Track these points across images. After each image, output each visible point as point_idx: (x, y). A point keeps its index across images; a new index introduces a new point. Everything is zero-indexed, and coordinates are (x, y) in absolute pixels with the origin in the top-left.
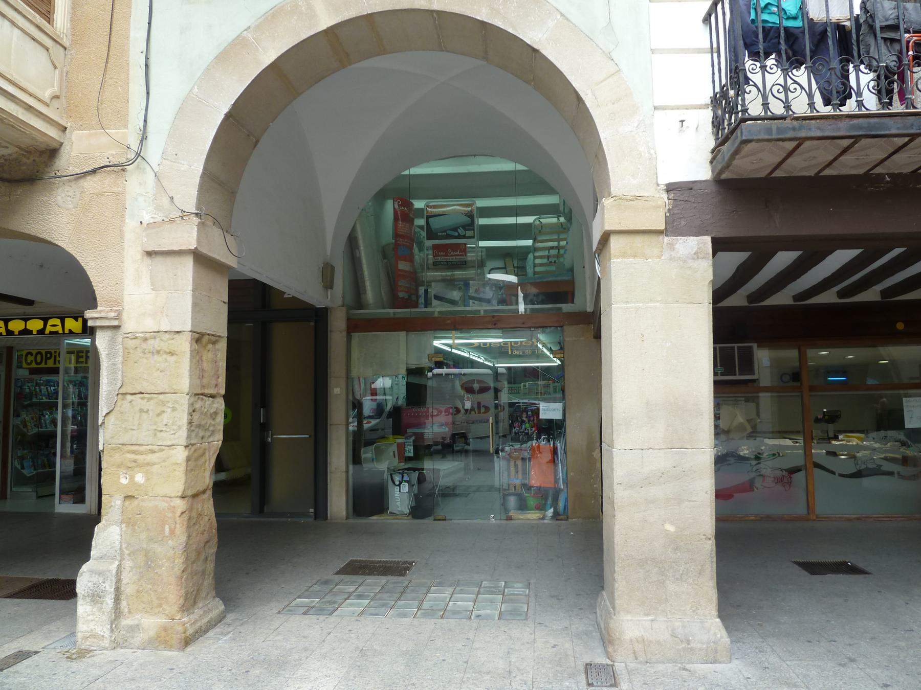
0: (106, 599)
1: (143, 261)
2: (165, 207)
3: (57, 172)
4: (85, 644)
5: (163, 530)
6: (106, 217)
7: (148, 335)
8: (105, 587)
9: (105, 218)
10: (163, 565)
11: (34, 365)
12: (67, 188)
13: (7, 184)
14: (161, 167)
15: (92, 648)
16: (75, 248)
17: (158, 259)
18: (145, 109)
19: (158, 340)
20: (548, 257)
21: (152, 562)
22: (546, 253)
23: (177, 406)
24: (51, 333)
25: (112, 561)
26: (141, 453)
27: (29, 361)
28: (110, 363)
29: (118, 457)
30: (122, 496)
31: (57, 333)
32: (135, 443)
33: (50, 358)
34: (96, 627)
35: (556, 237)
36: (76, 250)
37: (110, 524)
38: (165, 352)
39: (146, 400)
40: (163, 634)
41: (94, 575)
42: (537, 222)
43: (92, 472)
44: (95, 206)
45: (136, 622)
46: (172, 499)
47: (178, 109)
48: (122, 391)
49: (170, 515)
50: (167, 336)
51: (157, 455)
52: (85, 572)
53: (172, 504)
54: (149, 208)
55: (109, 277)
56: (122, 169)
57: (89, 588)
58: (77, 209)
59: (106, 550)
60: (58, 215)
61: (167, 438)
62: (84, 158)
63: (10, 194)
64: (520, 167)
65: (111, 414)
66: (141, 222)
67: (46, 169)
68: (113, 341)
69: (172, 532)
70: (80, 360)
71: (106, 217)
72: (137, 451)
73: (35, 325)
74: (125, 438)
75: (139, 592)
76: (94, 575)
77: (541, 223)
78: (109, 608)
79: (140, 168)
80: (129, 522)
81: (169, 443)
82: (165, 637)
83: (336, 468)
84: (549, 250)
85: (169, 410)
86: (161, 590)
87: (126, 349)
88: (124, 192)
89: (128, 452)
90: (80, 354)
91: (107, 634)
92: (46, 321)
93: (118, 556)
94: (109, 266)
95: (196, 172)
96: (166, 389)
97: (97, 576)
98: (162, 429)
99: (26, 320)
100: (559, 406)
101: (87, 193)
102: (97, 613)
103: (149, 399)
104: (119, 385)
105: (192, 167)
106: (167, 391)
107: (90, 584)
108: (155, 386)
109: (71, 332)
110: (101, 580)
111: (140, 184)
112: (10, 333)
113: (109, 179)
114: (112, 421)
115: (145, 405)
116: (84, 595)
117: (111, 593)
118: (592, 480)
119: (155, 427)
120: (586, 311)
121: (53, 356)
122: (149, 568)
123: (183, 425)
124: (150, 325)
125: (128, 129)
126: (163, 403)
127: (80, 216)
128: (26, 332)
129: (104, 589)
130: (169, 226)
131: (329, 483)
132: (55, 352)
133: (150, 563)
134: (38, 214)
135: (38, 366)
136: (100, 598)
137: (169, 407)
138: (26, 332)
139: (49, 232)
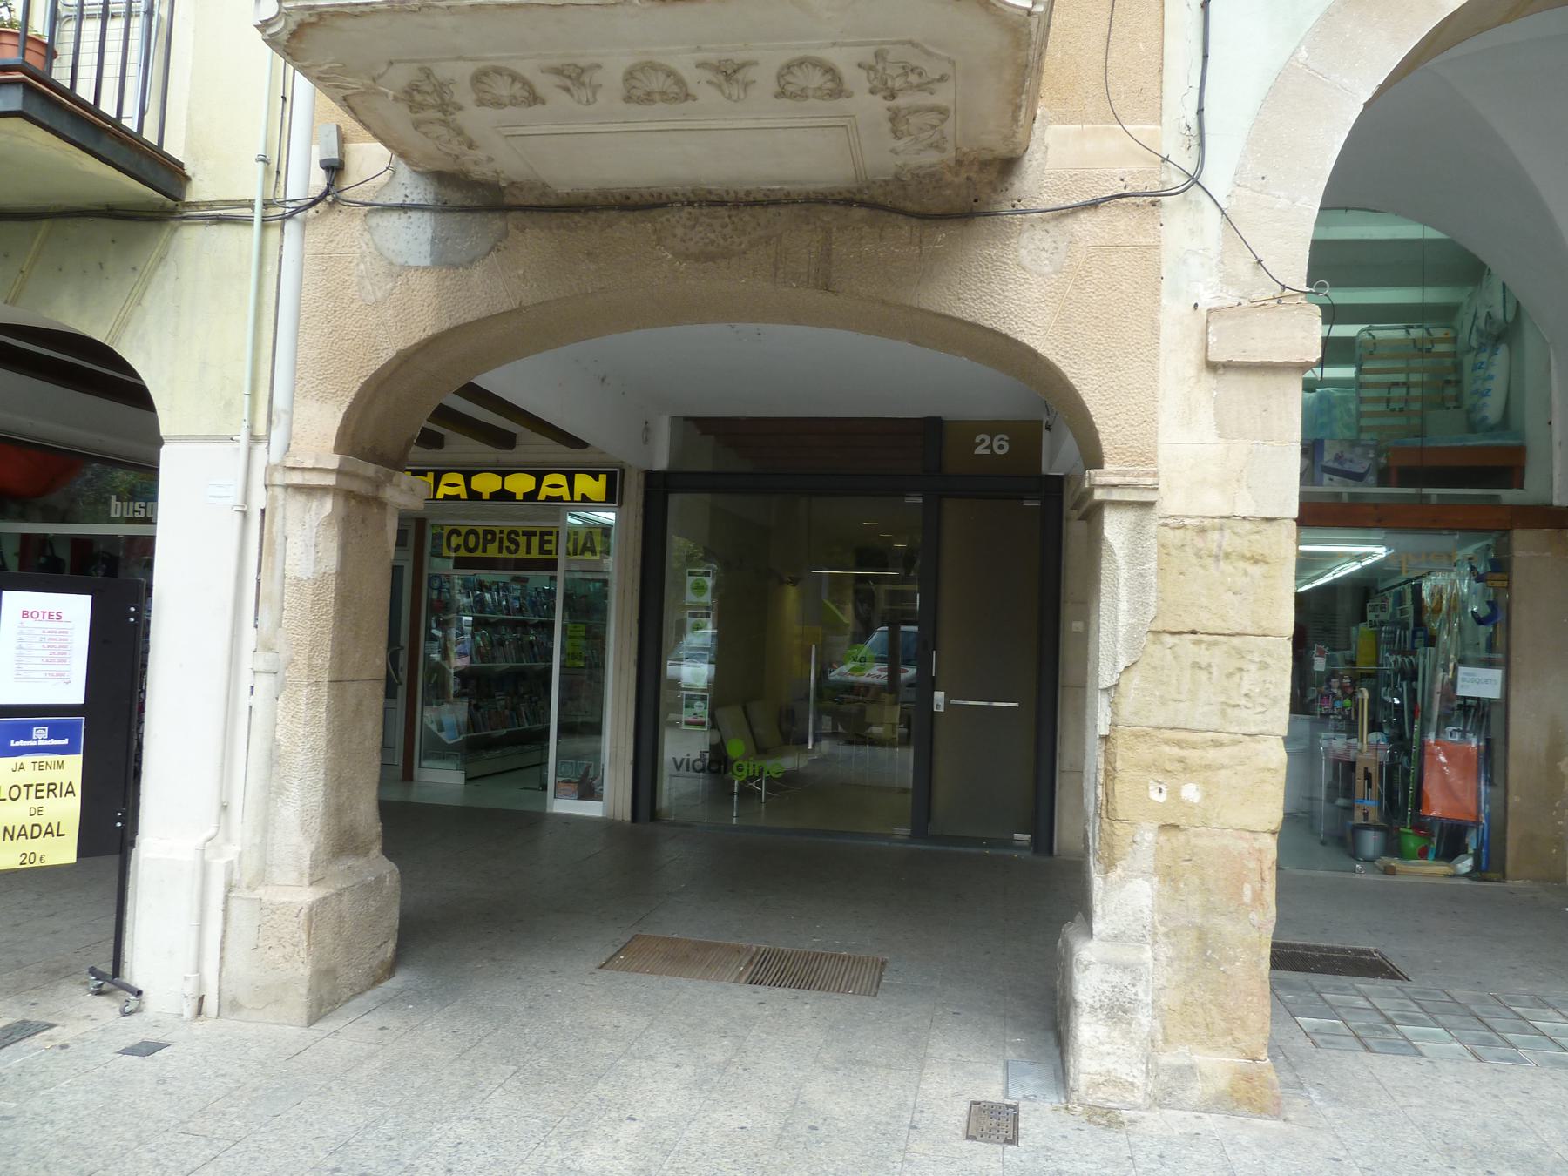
0: (1139, 1016)
1: (1199, 381)
2: (1242, 279)
3: (1016, 202)
4: (1094, 1096)
5: (1239, 892)
6: (1122, 292)
7: (1207, 522)
8: (1136, 994)
9: (1120, 295)
10: (1237, 959)
11: (463, 553)
12: (1039, 233)
13: (914, 221)
14: (1234, 202)
15: (1110, 1104)
16: (1057, 349)
17: (1232, 378)
18: (1198, 86)
19: (1227, 532)
20: (1388, 401)
21: (1214, 951)
22: (1383, 392)
23: (1268, 660)
24: (549, 498)
25: (1137, 944)
26: (1193, 746)
27: (454, 545)
28: (1133, 571)
29: (1144, 751)
30: (1156, 825)
31: (559, 499)
32: (1182, 726)
33: (493, 541)
34: (1117, 1066)
35: (1400, 364)
36: (1061, 353)
37: (1131, 876)
38: (1243, 557)
39: (1203, 646)
40: (1243, 1085)
41: (1112, 970)
42: (1365, 336)
43: (617, 747)
44: (1098, 271)
45: (1185, 1062)
46: (1256, 836)
47: (1267, 90)
48: (1158, 626)
49: (1252, 864)
50: (1247, 526)
51: (1227, 750)
52: (1094, 963)
53: (1256, 845)
54: (1209, 280)
55: (1129, 407)
56: (1151, 202)
57: (1104, 993)
58: (1060, 275)
59: (1125, 923)
60: (1021, 285)
61: (1251, 720)
62: (1071, 177)
63: (921, 242)
64: (1432, 234)
65: (1134, 668)
66: (1196, 305)
67: (995, 197)
68: (1138, 530)
69: (1257, 896)
70: (547, 547)
71: (1122, 292)
72: (1186, 741)
73: (520, 484)
74: (1159, 716)
75: (1186, 1005)
76: (1112, 970)
77: (1374, 337)
78: (1143, 1032)
79: (1191, 202)
80: (1168, 875)
81: (1253, 730)
82: (1247, 1093)
83: (1071, 766)
84: (1389, 388)
85: (1253, 667)
86: (1232, 1004)
87: (1163, 546)
88: (1157, 247)
89: (1166, 743)
90: (547, 538)
91: (1140, 1080)
92: (539, 477)
93: (1147, 937)
94: (1129, 387)
95: (1306, 213)
96: (1245, 628)
97: (1119, 972)
98: (1238, 703)
99: (503, 474)
100: (1496, 674)
101: (1081, 245)
102: (1120, 1041)
103: (1211, 645)
104: (1151, 616)
105: (1298, 204)
106: (1249, 630)
107: (1105, 987)
108: (1224, 620)
109: (585, 498)
110: (1127, 979)
111: (1192, 232)
112: (474, 496)
113: (1126, 219)
114: (1136, 681)
115: (1204, 656)
116: (1092, 1007)
117: (1147, 1004)
118: (1554, 813)
119: (1223, 699)
120: (1551, 505)
121: (497, 540)
122: (1206, 960)
123: (1283, 696)
124: (1213, 503)
125: (1161, 124)
126: (1240, 654)
127: (1067, 288)
128: (503, 495)
129: (1133, 997)
130: (1263, 315)
131: (1057, 789)
132: (501, 532)
133: (1209, 952)
134: (981, 281)
135: (513, 556)
136: (1125, 1012)
137: (1252, 662)
138: (503, 495)
139: (1004, 318)
